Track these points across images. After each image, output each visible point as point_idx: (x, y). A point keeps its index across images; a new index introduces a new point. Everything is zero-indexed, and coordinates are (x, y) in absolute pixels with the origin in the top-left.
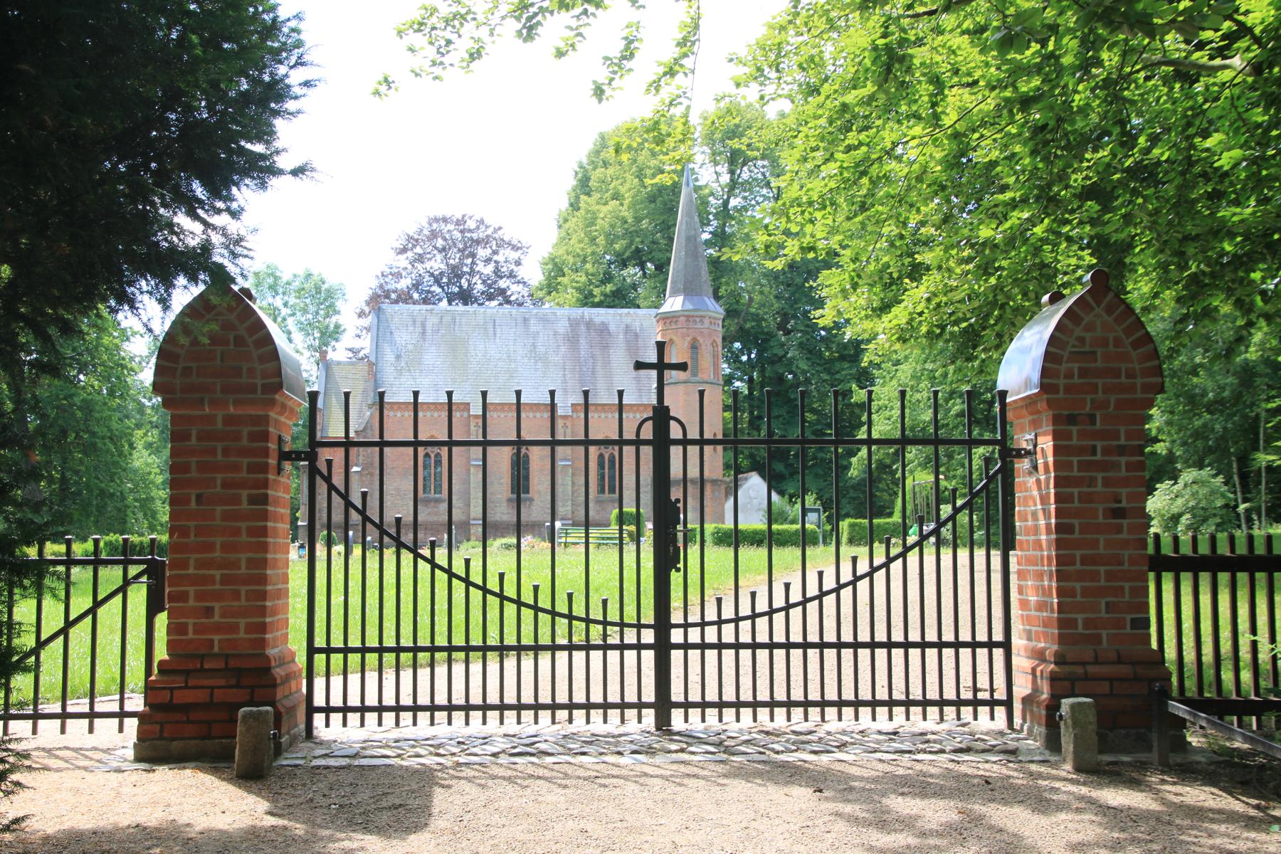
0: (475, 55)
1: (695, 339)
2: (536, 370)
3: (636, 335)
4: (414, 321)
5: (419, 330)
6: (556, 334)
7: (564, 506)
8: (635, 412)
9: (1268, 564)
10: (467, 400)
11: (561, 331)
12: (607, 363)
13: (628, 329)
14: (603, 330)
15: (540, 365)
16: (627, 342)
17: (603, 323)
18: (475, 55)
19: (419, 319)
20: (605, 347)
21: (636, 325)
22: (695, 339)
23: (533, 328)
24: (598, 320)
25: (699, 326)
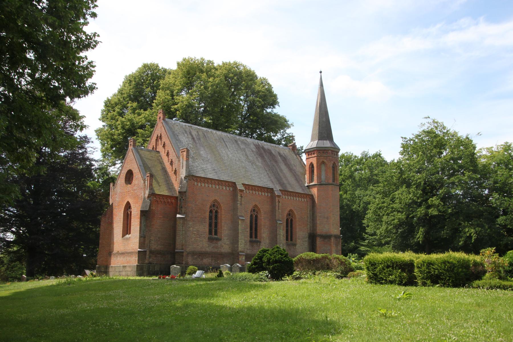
1: (334, 163)
5: (190, 136)
12: (281, 170)
20: (276, 162)
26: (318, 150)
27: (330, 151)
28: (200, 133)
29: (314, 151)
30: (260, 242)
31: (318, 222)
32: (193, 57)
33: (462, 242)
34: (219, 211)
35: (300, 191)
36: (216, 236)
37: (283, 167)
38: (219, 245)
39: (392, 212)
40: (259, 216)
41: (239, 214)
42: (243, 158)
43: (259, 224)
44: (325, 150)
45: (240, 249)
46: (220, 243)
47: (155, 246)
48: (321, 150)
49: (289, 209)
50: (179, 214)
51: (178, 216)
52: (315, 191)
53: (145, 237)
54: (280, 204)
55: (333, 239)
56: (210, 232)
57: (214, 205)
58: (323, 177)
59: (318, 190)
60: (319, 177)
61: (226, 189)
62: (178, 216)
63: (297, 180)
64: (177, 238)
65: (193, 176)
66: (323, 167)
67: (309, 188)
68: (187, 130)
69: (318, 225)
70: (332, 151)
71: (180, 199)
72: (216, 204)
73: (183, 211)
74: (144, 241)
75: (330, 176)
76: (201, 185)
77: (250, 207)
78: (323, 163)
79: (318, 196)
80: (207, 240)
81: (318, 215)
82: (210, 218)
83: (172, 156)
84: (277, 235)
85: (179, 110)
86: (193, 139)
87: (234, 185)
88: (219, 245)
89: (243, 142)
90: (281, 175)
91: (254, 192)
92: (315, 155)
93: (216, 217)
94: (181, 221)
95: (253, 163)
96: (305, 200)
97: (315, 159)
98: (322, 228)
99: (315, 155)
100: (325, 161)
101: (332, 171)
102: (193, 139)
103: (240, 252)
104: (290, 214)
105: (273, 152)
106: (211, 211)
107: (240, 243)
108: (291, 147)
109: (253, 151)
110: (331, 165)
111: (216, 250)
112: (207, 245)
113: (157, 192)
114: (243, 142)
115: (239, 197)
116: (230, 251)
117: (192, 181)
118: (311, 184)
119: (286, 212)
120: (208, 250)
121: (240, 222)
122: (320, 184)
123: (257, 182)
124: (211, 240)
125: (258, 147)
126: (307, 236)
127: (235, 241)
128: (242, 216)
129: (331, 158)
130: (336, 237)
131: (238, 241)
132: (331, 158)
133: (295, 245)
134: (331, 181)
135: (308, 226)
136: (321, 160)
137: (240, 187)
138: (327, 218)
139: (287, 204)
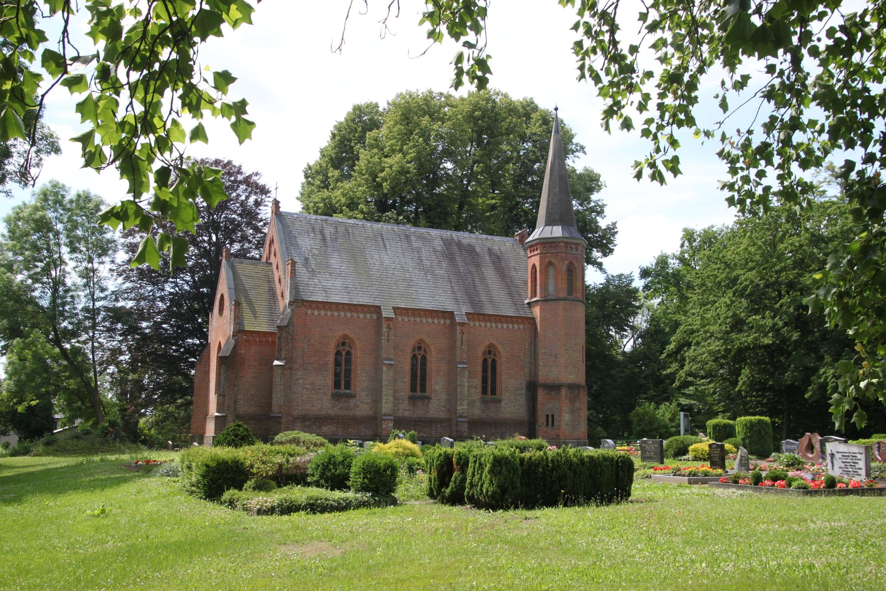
0: (723, 83)
1: (571, 264)
2: (428, 281)
3: (498, 257)
4: (313, 229)
5: (319, 237)
6: (435, 251)
7: (461, 404)
8: (513, 323)
9: (881, 492)
10: (377, 303)
11: (439, 248)
12: (483, 279)
13: (490, 252)
14: (471, 250)
15: (429, 277)
16: (493, 262)
17: (469, 245)
18: (723, 83)
19: (317, 227)
20: (478, 265)
21: (496, 248)
22: (571, 264)
23: (415, 245)
24: (465, 242)
25: (574, 252)
26: (542, 244)
27: (562, 244)
28: (341, 230)
29: (537, 244)
30: (429, 398)
31: (541, 363)
32: (413, 90)
33: (809, 394)
34: (353, 352)
35: (510, 312)
36: (348, 391)
37: (490, 273)
38: (352, 404)
39: (706, 339)
40: (428, 357)
41: (384, 355)
42: (411, 264)
43: (428, 370)
44: (554, 242)
45: (384, 411)
46: (352, 402)
47: (244, 408)
48: (547, 243)
49: (487, 343)
50: (278, 359)
51: (276, 363)
52: (537, 311)
53: (224, 396)
54: (465, 337)
55: (564, 391)
56: (337, 385)
57: (343, 344)
58: (551, 288)
59: (541, 309)
60: (544, 287)
61: (365, 317)
62: (276, 363)
63: (510, 294)
64: (274, 396)
65: (303, 300)
66: (551, 272)
67: (530, 307)
68: (317, 227)
69: (540, 368)
70: (566, 243)
71: (280, 338)
72: (347, 341)
73: (283, 356)
74: (224, 402)
75: (563, 285)
76: (319, 314)
77: (410, 344)
78: (550, 263)
79: (541, 320)
80: (330, 397)
81: (541, 350)
82: (337, 363)
83: (281, 273)
84: (456, 387)
85: (386, 180)
86: (324, 239)
87: (377, 309)
88: (352, 404)
89: (421, 237)
90: (480, 287)
91: (418, 319)
92: (539, 251)
93: (348, 361)
94: (279, 371)
95: (427, 271)
96: (521, 327)
97: (538, 258)
98: (548, 373)
99: (539, 251)
100: (554, 261)
101: (565, 277)
102: (324, 239)
103: (385, 415)
104: (491, 351)
105: (478, 249)
106: (338, 353)
107: (384, 401)
108: (518, 238)
109: (435, 251)
110: (564, 267)
111: (346, 413)
112: (330, 406)
113: (248, 327)
114: (421, 237)
115: (384, 329)
116: (371, 413)
117: (303, 308)
118: (534, 299)
119: (481, 349)
120: (331, 412)
121: (384, 368)
122: (545, 300)
123: (426, 303)
124: (336, 397)
125: (447, 243)
126: (524, 385)
127: (377, 400)
128: (391, 360)
129: (564, 255)
130: (572, 387)
131: (381, 398)
132: (564, 255)
133: (499, 401)
134: (563, 294)
135: (527, 370)
136: (547, 260)
137: (387, 313)
138: (556, 356)
139: (487, 335)
